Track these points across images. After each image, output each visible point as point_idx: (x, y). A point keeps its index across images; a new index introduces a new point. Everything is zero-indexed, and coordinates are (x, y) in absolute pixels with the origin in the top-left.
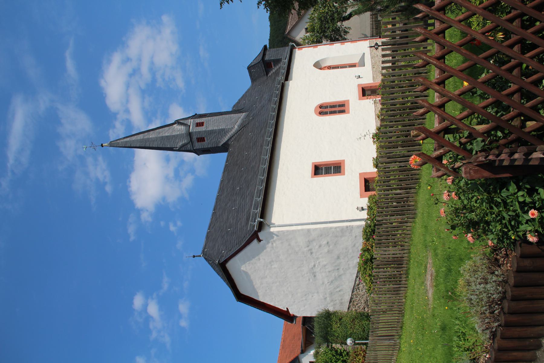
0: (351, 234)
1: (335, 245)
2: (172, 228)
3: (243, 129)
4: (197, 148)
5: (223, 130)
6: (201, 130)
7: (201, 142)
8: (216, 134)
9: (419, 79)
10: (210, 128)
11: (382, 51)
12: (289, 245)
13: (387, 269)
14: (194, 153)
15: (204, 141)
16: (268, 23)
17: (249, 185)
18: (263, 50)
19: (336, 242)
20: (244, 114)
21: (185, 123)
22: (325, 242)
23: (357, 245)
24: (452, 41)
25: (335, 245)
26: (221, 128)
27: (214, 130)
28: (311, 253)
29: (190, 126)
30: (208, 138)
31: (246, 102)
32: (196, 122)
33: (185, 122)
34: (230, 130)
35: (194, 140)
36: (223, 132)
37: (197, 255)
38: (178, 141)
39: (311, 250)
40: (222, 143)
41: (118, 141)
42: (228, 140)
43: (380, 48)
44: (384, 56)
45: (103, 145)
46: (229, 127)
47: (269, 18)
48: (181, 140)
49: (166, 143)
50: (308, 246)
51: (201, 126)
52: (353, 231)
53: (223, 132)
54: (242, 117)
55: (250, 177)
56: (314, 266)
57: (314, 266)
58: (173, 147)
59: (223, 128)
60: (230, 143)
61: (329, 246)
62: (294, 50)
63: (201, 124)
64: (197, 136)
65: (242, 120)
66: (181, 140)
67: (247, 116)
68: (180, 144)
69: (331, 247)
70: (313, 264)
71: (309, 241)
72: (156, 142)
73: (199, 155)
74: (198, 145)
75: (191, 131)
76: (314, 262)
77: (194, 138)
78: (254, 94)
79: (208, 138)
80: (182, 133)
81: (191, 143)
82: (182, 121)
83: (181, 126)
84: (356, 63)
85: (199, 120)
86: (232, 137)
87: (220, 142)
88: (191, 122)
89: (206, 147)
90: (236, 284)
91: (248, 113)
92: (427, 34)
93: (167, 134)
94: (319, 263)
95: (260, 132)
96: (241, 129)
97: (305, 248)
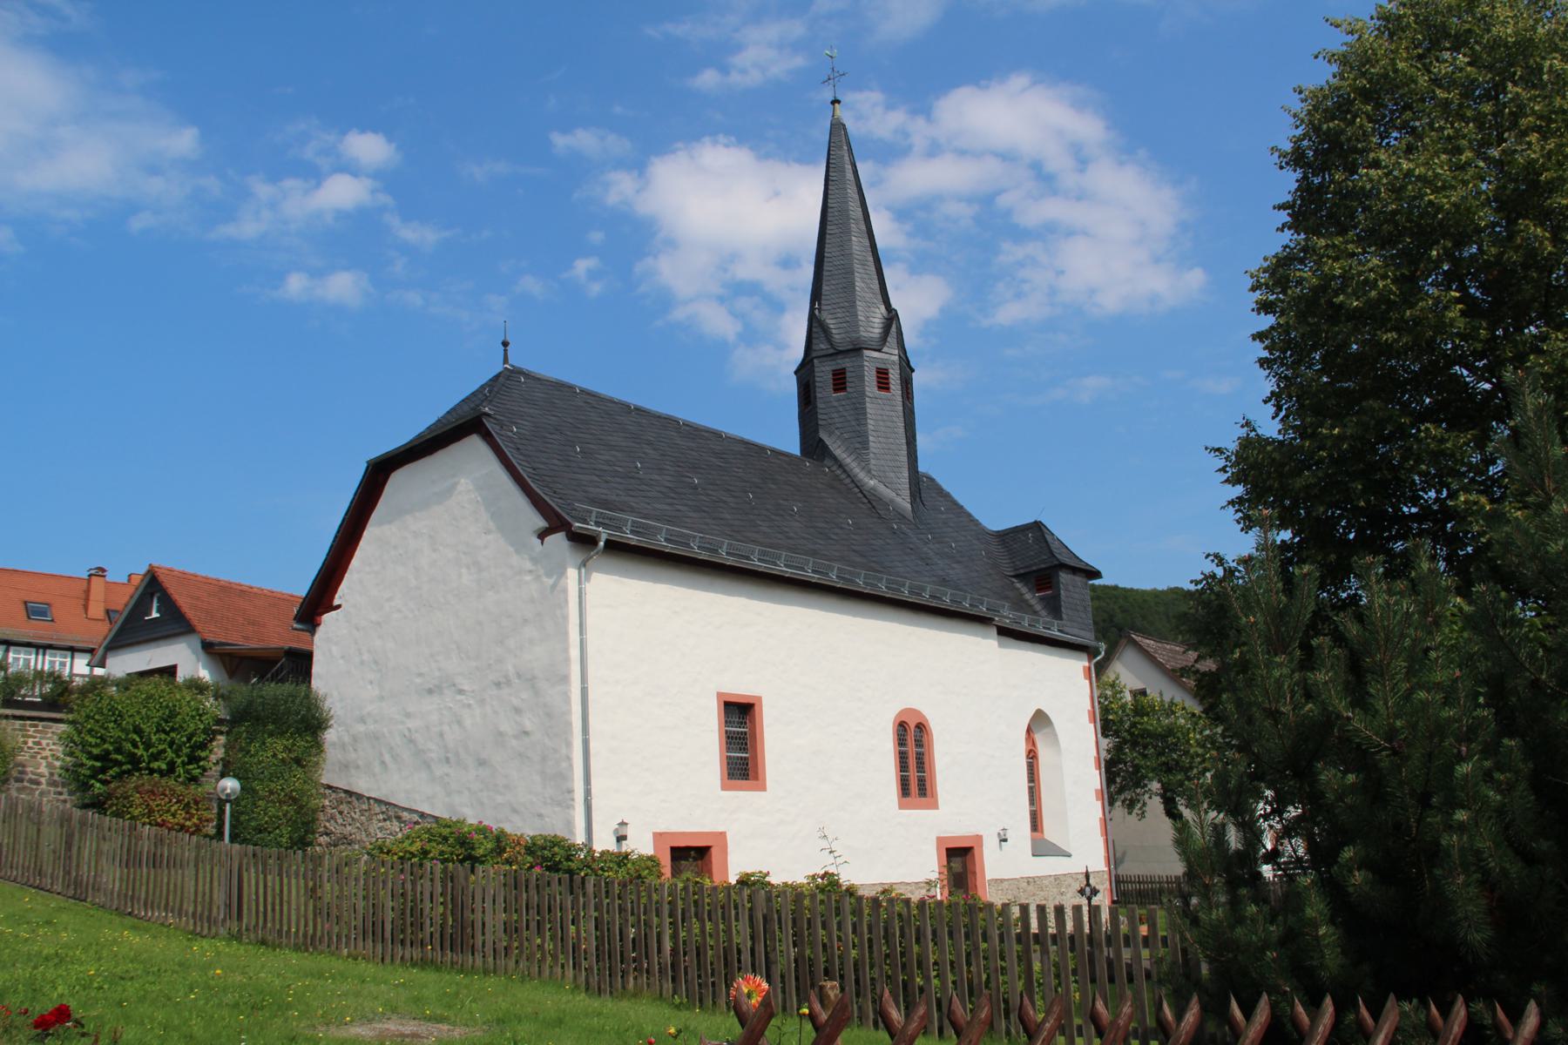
2: (582, 266)
3: (866, 501)
4: (816, 369)
5: (865, 444)
6: (867, 383)
7: (834, 380)
8: (853, 423)
10: (870, 408)
11: (1038, 906)
14: (804, 360)
15: (836, 390)
17: (704, 511)
18: (1088, 568)
19: (528, 758)
20: (909, 506)
21: (889, 339)
26: (871, 438)
27: (866, 419)
28: (498, 685)
29: (879, 351)
30: (843, 403)
31: (942, 513)
32: (891, 371)
33: (892, 339)
34: (863, 464)
35: (839, 361)
36: (858, 446)
38: (839, 315)
40: (828, 441)
41: (845, 148)
42: (835, 459)
44: (1059, 910)
45: (837, 105)
46: (873, 462)
48: (841, 325)
49: (833, 282)
50: (519, 676)
51: (878, 382)
53: (858, 446)
54: (899, 500)
55: (728, 516)
56: (461, 692)
57: (461, 692)
58: (823, 302)
59: (871, 444)
60: (827, 462)
61: (516, 737)
62: (1085, 656)
63: (883, 383)
64: (852, 369)
65: (892, 501)
66: (841, 325)
67: (901, 517)
68: (828, 321)
70: (466, 688)
72: (838, 253)
73: (796, 373)
74: (823, 372)
75: (866, 353)
77: (846, 363)
78: (963, 538)
79: (843, 403)
80: (861, 328)
81: (832, 351)
82: (894, 329)
83: (881, 326)
84: (1042, 832)
85: (894, 377)
86: (845, 471)
87: (831, 434)
88: (890, 355)
89: (818, 395)
90: (780, 603)
91: (911, 519)
93: (859, 284)
94: (469, 706)
95: (854, 551)
96: (865, 496)
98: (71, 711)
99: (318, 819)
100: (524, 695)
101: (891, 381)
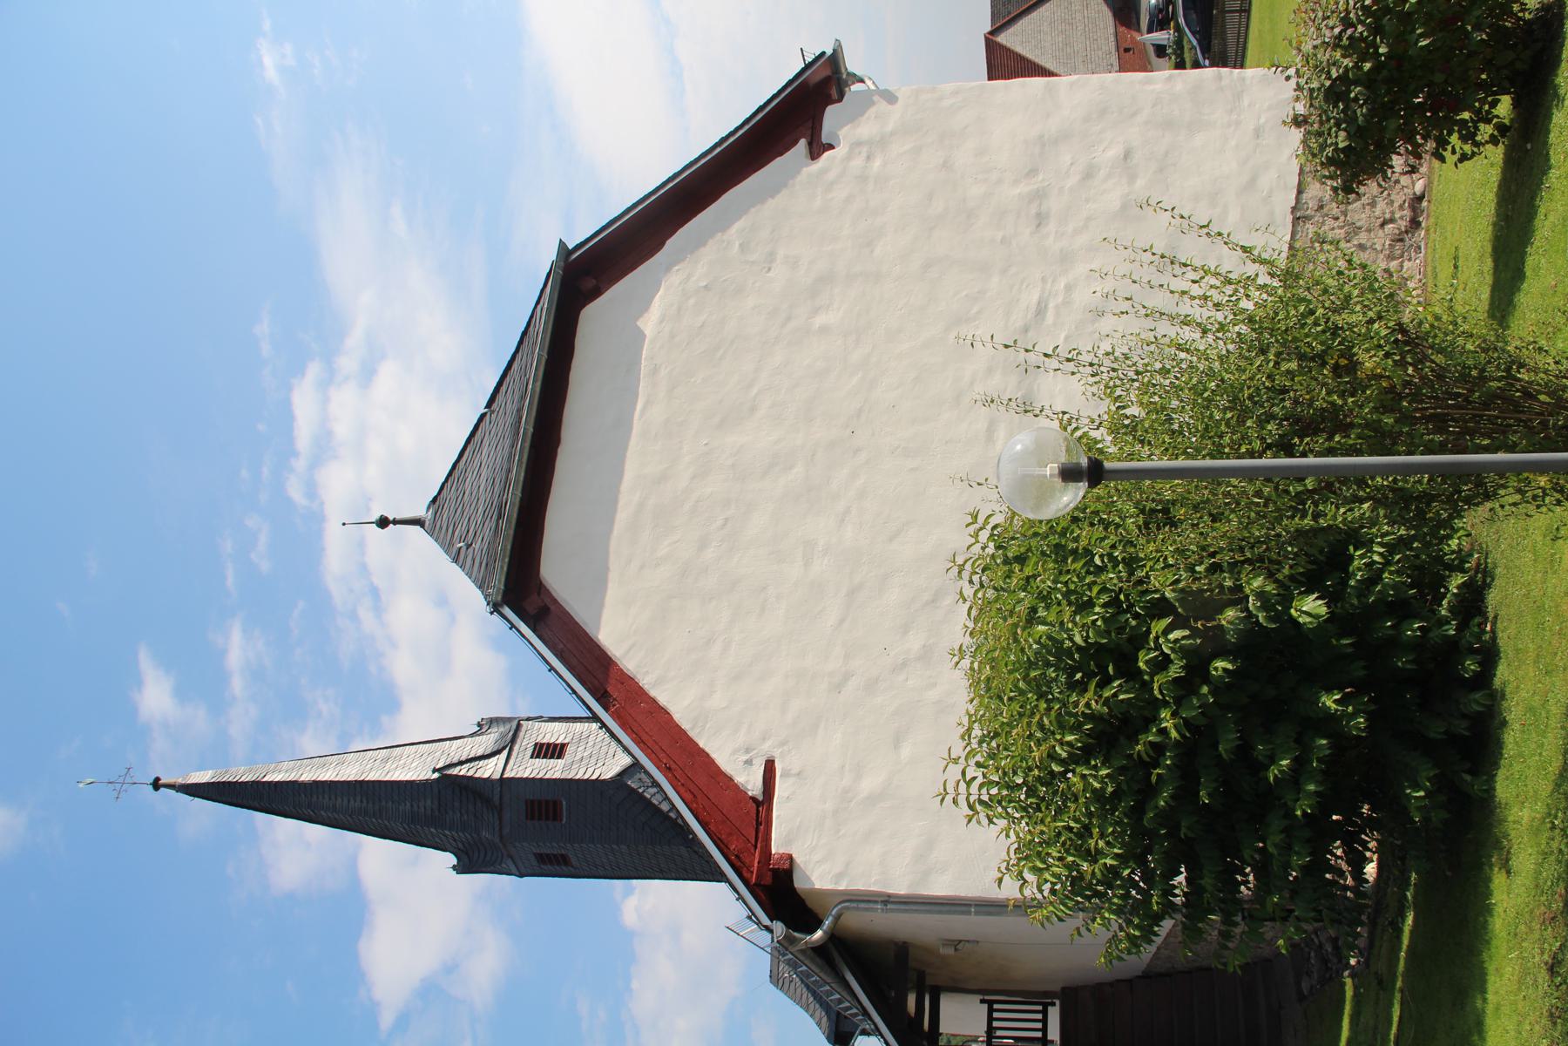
0: (1234, 117)
10: (581, 773)
12: (946, 165)
19: (1167, 154)
22: (1115, 152)
23: (1266, 181)
24: (1550, 950)
28: (1041, 219)
37: (399, 517)
39: (1039, 195)
50: (1033, 172)
56: (1041, 311)
57: (1041, 311)
61: (1132, 178)
70: (1035, 298)
71: (1041, 137)
76: (1044, 280)
90: (567, 400)
92: (1427, 408)
94: (1069, 288)
97: (1016, 182)
98: (754, 749)
99: (1358, 363)
100: (1067, 159)
101: (545, 741)
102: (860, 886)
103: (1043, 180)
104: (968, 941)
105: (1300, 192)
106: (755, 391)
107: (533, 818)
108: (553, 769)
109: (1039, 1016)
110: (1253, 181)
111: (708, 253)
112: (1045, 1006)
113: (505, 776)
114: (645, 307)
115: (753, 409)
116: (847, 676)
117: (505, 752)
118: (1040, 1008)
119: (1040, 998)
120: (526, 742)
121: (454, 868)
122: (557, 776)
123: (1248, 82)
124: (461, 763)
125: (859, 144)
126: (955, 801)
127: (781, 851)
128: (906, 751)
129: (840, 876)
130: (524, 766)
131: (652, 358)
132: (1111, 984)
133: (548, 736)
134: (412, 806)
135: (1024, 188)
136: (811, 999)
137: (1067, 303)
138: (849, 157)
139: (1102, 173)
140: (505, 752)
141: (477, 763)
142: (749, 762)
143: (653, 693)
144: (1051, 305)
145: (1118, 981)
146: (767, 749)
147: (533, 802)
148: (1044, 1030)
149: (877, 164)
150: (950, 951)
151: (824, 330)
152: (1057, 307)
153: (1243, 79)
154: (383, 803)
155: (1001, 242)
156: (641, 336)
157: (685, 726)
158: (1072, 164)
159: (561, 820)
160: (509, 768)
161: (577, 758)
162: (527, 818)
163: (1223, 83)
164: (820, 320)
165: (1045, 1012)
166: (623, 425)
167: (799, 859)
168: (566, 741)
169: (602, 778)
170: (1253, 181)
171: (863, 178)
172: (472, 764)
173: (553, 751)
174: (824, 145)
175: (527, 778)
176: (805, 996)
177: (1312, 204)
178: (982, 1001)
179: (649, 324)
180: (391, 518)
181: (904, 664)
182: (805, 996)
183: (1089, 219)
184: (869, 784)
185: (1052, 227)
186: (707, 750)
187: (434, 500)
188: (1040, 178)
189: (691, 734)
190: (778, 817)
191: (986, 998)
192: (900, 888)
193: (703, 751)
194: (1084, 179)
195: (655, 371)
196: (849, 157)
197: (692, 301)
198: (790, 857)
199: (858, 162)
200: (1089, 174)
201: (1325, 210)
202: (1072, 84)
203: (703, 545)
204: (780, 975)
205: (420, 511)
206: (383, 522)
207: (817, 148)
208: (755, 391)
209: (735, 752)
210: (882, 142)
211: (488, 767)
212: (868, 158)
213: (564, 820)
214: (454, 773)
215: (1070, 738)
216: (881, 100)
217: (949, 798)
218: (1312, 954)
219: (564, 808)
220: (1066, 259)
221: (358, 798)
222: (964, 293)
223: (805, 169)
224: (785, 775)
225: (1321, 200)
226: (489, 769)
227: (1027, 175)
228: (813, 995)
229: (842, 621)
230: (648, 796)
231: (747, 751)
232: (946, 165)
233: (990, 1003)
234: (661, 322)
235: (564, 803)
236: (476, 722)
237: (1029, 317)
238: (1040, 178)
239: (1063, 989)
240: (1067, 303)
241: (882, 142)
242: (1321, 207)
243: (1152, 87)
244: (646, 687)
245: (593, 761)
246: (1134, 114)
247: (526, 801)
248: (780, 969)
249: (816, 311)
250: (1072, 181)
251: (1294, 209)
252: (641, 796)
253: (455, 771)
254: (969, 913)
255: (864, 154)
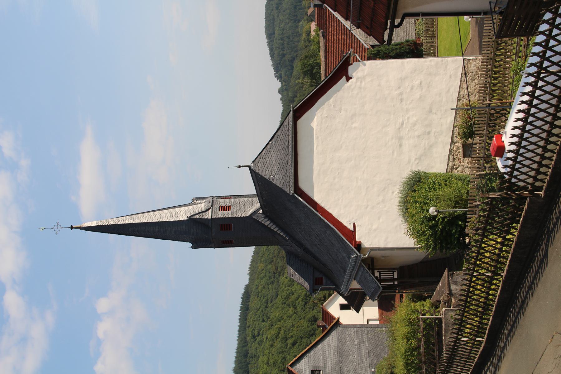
1: (428, 87)
9: (324, 278)
12: (379, 85)
13: (521, 52)
16: (265, 14)
22: (418, 82)
23: (452, 90)
25: (428, 87)
28: (402, 100)
43: (311, 311)
47: (281, 114)
50: (399, 88)
52: (448, 68)
56: (402, 124)
57: (402, 124)
61: (422, 89)
69: (424, 90)
70: (401, 121)
71: (401, 78)
94: (408, 118)
102: (375, 246)
103: (402, 90)
104: (387, 256)
105: (459, 92)
106: (341, 143)
107: (222, 230)
108: (228, 214)
109: (392, 274)
110: (449, 90)
111: (326, 106)
112: (393, 272)
113: (213, 217)
114: (313, 119)
115: (341, 147)
116: (368, 206)
117: (211, 209)
118: (392, 272)
119: (392, 270)
120: (217, 206)
121: (191, 247)
122: (230, 216)
123: (449, 62)
124: (197, 214)
125: (358, 78)
126: (406, 235)
127: (358, 241)
128: (381, 220)
129: (370, 245)
130: (218, 214)
131: (317, 135)
132: (412, 265)
133: (223, 204)
134: (178, 228)
135: (398, 92)
136: (303, 280)
137: (408, 122)
138: (356, 82)
139: (415, 88)
140: (211, 209)
141: (202, 214)
142: (350, 224)
143: (328, 211)
144: (405, 122)
145: (414, 264)
146: (354, 221)
147: (222, 225)
148: (393, 276)
149: (363, 84)
150: (383, 258)
151: (355, 128)
152: (406, 123)
153: (447, 61)
154: (167, 228)
155: (393, 106)
156: (312, 129)
157: (336, 217)
158: (408, 85)
159: (232, 230)
160: (213, 215)
161: (235, 210)
162: (220, 230)
163: (443, 62)
164: (354, 125)
165: (393, 273)
166: (312, 151)
167: (362, 242)
168: (230, 205)
169: (245, 216)
170: (449, 90)
171: (360, 88)
172: (200, 214)
173: (227, 208)
174: (349, 77)
175: (220, 218)
176: (301, 279)
177: (462, 96)
178: (378, 272)
179: (315, 124)
180: (241, 166)
181: (379, 203)
182: (301, 279)
183: (412, 100)
184: (374, 227)
185: (404, 103)
186: (341, 222)
187: (253, 162)
188: (401, 89)
189: (337, 219)
190: (357, 234)
191: (379, 271)
192: (382, 246)
193: (340, 222)
194: (411, 90)
195: (318, 138)
196: (356, 82)
197: (324, 120)
198: (360, 242)
199: (359, 83)
200: (412, 89)
201: (464, 97)
202: (408, 62)
203: (334, 179)
204: (291, 273)
205: (249, 163)
206: (239, 167)
207: (348, 78)
208: (341, 143)
209: (347, 222)
210: (364, 78)
211: (206, 215)
212: (361, 82)
213: (233, 230)
214: (195, 218)
215: (427, 228)
216: (363, 65)
217: (405, 234)
218: (458, 255)
219: (233, 226)
220: (408, 110)
221: (157, 227)
222: (385, 119)
223: (346, 84)
224: (358, 226)
225: (464, 95)
226: (208, 215)
227: (398, 88)
228: (303, 279)
229: (366, 194)
230: (261, 221)
231: (350, 221)
232: (379, 85)
233: (380, 272)
234: (317, 126)
235: (233, 224)
236: (191, 199)
237: (400, 126)
238: (401, 89)
239: (401, 267)
240: (408, 122)
241: (364, 78)
242: (464, 97)
243: (427, 63)
244: (327, 210)
245: (240, 210)
246: (422, 71)
247: (220, 225)
248: (291, 271)
249: (353, 123)
250: (408, 90)
251: (458, 97)
252: (258, 221)
253: (195, 217)
254: (377, 251)
255: (360, 81)
